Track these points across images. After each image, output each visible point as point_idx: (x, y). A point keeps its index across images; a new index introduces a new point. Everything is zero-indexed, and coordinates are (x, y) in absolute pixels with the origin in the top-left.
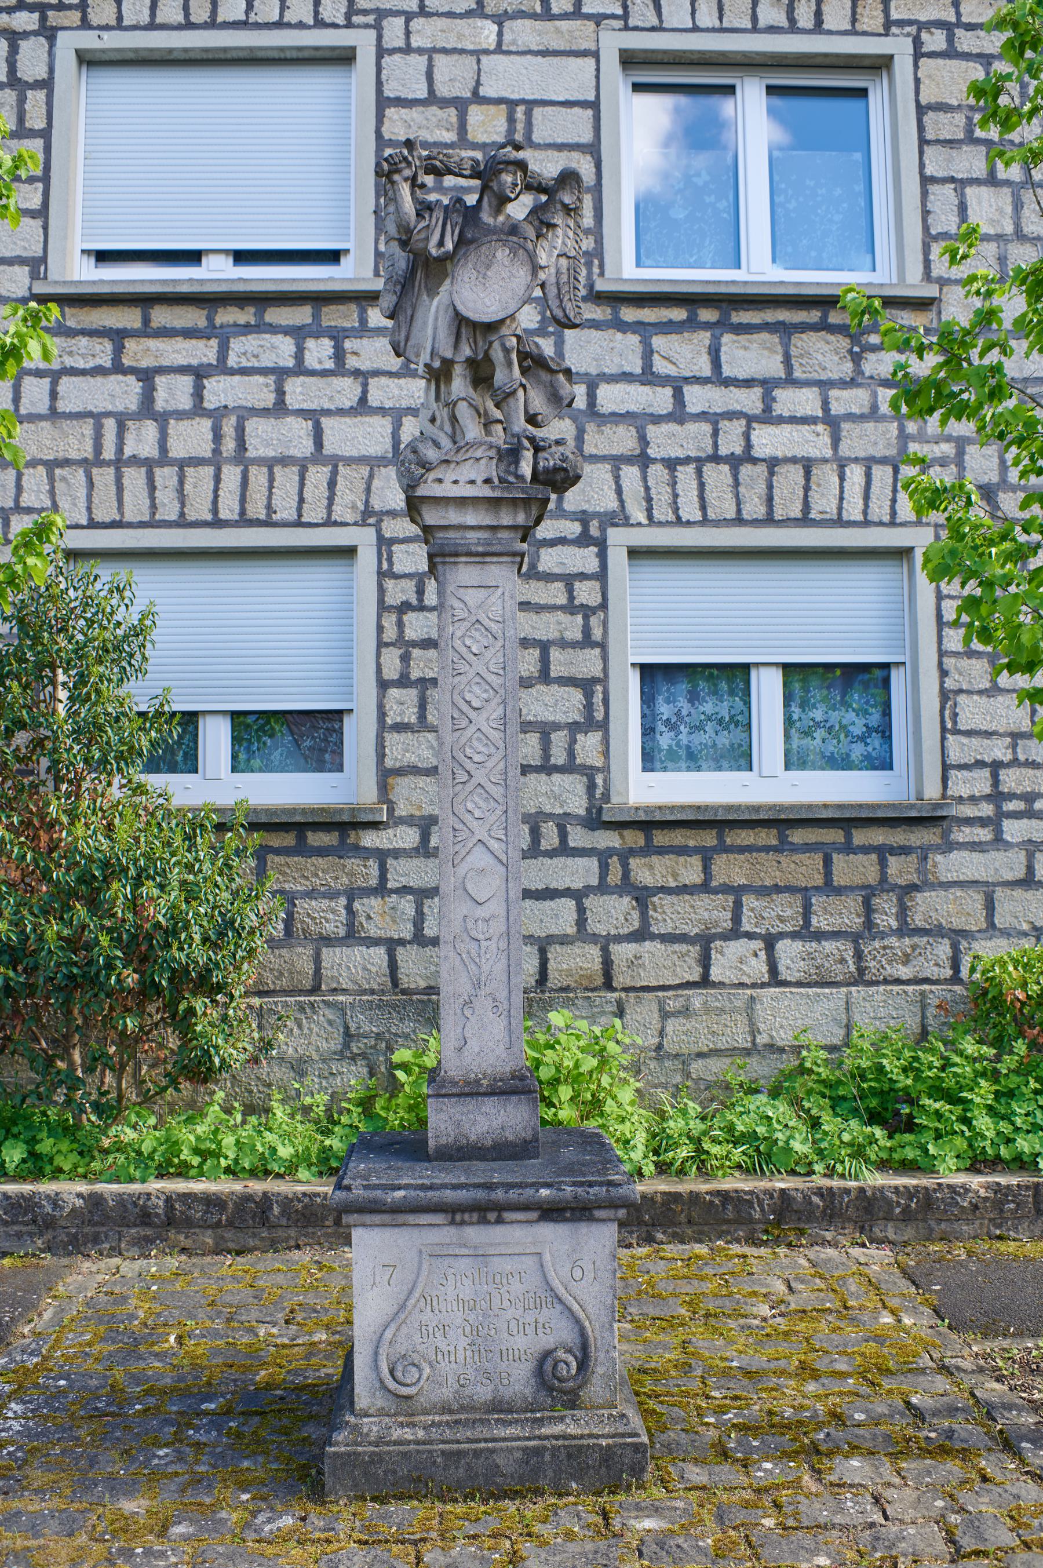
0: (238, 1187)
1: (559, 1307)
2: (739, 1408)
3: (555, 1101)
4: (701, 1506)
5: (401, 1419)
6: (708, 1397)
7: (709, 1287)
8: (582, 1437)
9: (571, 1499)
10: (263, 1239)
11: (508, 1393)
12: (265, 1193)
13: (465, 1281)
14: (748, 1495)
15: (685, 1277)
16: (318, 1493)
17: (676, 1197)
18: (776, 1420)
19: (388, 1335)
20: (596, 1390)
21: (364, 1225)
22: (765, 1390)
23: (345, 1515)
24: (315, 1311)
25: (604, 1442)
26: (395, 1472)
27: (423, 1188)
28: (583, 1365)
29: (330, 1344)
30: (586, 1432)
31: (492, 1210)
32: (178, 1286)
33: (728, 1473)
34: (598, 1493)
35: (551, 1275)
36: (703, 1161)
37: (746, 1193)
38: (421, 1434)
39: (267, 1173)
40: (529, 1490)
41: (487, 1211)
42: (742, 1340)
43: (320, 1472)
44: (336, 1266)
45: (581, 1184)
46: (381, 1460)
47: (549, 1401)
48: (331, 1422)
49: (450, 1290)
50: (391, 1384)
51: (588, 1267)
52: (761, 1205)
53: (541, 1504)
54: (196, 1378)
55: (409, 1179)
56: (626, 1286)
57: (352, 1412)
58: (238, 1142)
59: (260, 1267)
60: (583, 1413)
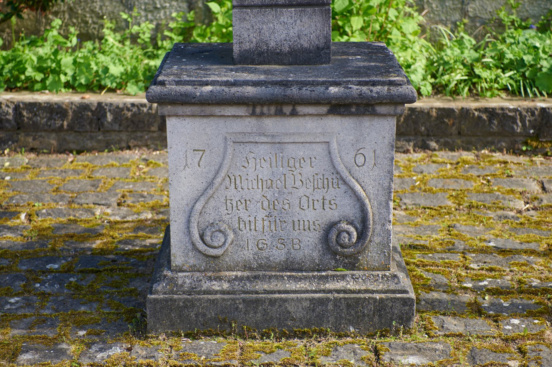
0: (76, 98)
1: (343, 187)
2: (494, 277)
3: (347, 29)
4: (457, 349)
5: (209, 274)
6: (467, 268)
7: (474, 185)
8: (359, 292)
9: (349, 339)
10: (99, 141)
11: (299, 256)
12: (99, 104)
13: (264, 164)
14: (497, 342)
15: (453, 177)
16: (142, 331)
17: (448, 112)
18: (524, 287)
19: (199, 206)
20: (372, 254)
21: (177, 116)
22: (517, 264)
23: (164, 347)
24: (143, 196)
25: (378, 296)
26: (204, 315)
27: (227, 84)
28: (362, 234)
29: (154, 221)
30: (363, 288)
31: (288, 104)
32: (28, 177)
33: (480, 325)
34: (372, 336)
35: (337, 160)
36: (474, 84)
37: (510, 110)
38: (226, 286)
39: (101, 88)
40: (314, 332)
41: (281, 104)
42: (499, 227)
43: (144, 315)
44: (160, 163)
45: (366, 83)
46: (193, 305)
47: (333, 263)
48: (152, 277)
49: (251, 170)
50: (201, 246)
51: (370, 155)
52: (523, 120)
53: (324, 342)
54: (43, 245)
55: (218, 78)
56: (403, 183)
57: (169, 268)
58: (75, 62)
59: (97, 162)
60: (361, 273)
